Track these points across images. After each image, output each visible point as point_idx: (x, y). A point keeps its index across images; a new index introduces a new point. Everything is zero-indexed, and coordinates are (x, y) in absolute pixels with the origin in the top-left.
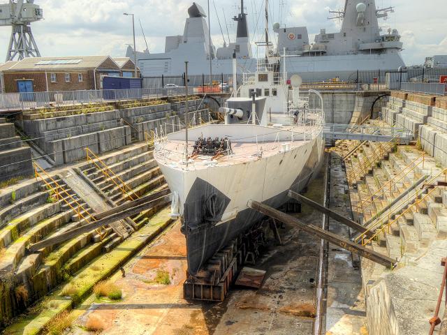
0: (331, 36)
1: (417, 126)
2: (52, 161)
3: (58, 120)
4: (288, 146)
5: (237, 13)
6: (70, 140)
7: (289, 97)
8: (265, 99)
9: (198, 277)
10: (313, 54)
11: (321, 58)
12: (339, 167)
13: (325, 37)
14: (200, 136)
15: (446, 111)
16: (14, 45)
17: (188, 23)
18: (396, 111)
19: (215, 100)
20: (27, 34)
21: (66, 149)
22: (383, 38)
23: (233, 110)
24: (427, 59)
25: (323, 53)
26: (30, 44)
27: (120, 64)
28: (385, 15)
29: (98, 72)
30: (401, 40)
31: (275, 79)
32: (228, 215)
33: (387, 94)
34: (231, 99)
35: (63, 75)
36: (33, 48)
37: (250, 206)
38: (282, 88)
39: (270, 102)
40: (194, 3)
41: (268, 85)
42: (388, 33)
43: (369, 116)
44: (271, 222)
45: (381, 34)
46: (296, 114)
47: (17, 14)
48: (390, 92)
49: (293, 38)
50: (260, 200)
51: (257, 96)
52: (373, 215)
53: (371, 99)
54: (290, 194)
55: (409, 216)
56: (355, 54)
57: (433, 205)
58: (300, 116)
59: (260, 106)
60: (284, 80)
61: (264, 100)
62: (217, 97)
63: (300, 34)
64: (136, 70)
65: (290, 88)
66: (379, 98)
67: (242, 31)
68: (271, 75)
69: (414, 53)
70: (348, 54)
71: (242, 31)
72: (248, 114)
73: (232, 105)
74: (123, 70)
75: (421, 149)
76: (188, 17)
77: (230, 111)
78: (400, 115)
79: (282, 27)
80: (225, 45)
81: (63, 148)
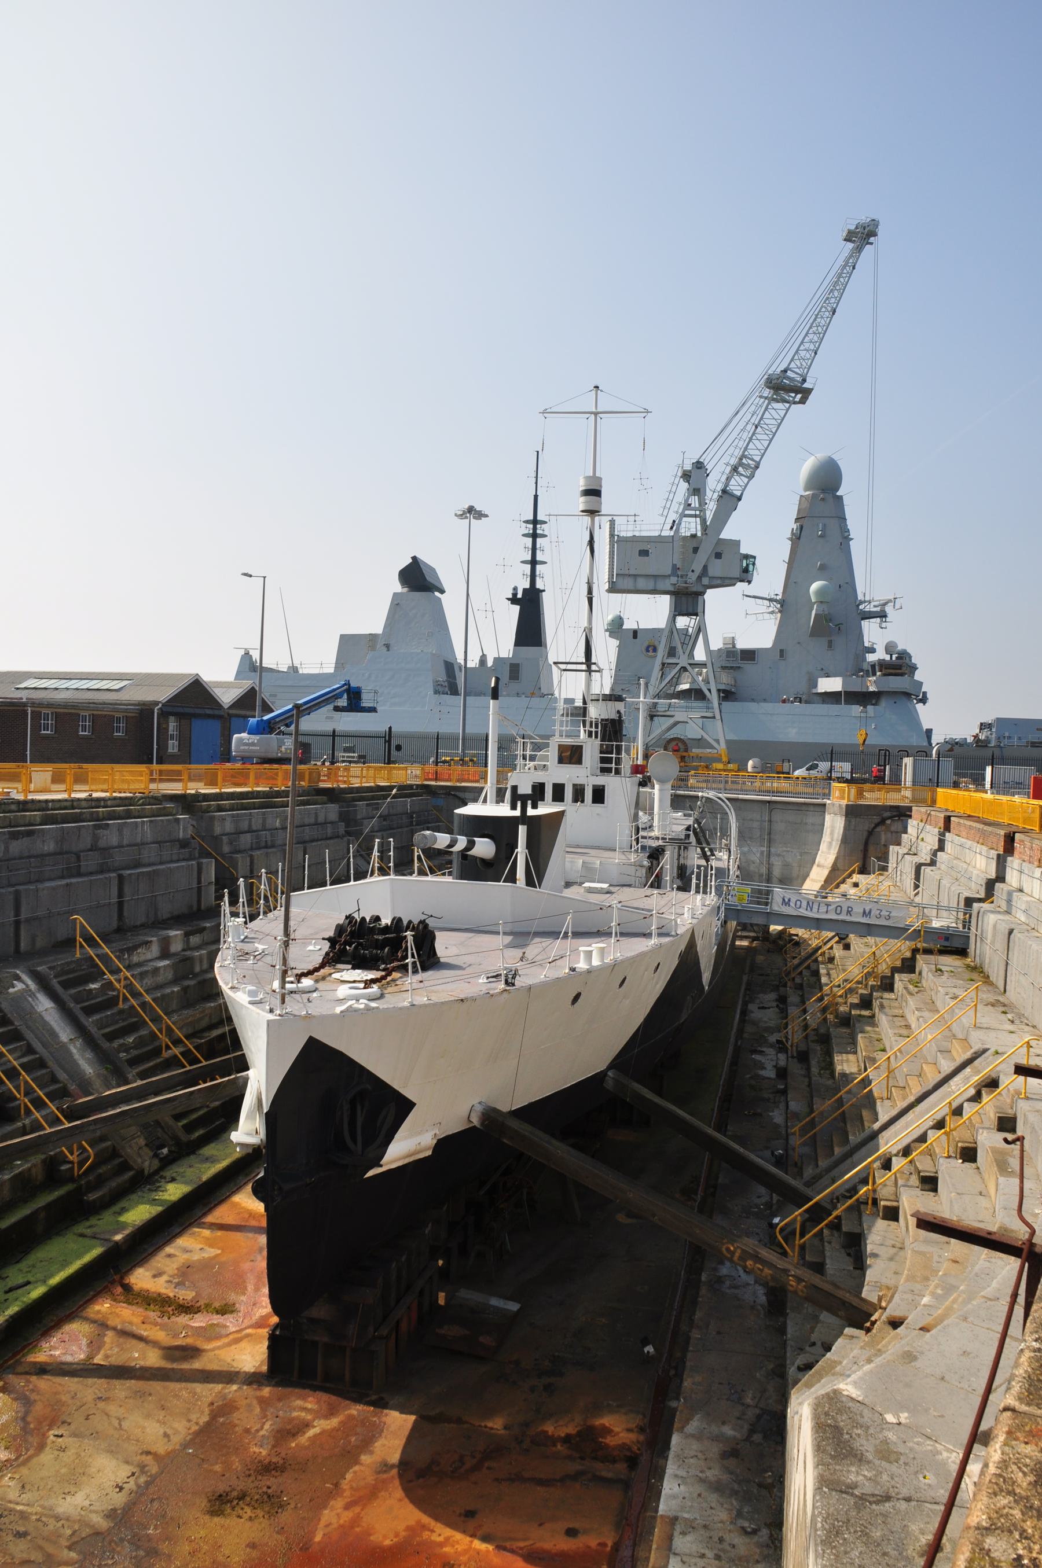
0: (749, 655)
1: (969, 902)
3: (14, 836)
4: (592, 955)
9: (312, 1321)
12: (770, 998)
15: (1037, 872)
17: (397, 603)
18: (924, 857)
21: (23, 916)
22: (873, 666)
24: (983, 726)
27: (227, 698)
28: (882, 615)
30: (918, 676)
31: (603, 760)
32: (406, 1146)
33: (902, 814)
37: (476, 1121)
38: (620, 788)
39: (578, 820)
40: (414, 558)
41: (585, 774)
42: (888, 658)
45: (871, 658)
48: (910, 809)
50: (505, 1108)
52: (823, 1163)
54: (609, 1084)
55: (926, 1166)
59: (543, 834)
61: (557, 818)
67: (530, 630)
69: (949, 715)
71: (530, 630)
72: (505, 848)
74: (231, 712)
75: (978, 970)
76: (398, 588)
81: (17, 913)
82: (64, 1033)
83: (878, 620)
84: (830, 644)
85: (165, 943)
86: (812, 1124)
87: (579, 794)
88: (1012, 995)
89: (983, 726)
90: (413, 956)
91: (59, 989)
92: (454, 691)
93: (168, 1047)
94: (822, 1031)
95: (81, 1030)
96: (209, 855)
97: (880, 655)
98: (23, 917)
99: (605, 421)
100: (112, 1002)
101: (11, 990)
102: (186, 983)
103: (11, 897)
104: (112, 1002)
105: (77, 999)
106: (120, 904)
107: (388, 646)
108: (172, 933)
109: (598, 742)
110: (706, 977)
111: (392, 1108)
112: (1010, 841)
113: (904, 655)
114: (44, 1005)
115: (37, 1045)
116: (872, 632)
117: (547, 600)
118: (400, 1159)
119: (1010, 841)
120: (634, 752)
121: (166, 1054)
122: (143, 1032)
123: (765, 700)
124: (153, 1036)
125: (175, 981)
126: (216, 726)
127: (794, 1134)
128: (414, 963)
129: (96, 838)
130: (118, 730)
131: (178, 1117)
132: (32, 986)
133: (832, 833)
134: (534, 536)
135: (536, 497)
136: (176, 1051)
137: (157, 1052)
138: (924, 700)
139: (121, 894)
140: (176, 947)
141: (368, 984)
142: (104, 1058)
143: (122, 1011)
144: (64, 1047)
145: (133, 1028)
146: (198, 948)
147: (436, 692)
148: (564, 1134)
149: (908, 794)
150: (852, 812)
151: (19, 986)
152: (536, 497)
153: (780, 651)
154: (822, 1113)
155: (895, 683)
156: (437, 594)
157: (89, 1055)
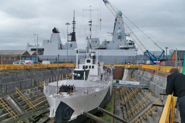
0: (108, 42)
2: (2, 92)
6: (25, 81)
7: (99, 69)
8: (89, 70)
11: (104, 50)
14: (63, 84)
17: (52, 35)
19: (69, 69)
23: (76, 74)
25: (105, 49)
31: (93, 62)
32: (74, 117)
34: (75, 70)
37: (82, 114)
40: (55, 28)
41: (91, 64)
43: (130, 77)
44: (91, 119)
46: (102, 76)
49: (92, 43)
51: (86, 69)
53: (131, 71)
54: (98, 109)
56: (117, 49)
57: (154, 113)
58: (103, 77)
59: (87, 72)
60: (97, 62)
62: (69, 68)
63: (96, 41)
64: (37, 56)
65: (99, 65)
66: (134, 70)
67: (73, 39)
68: (92, 60)
70: (115, 49)
73: (75, 72)
75: (150, 91)
76: (52, 32)
77: (75, 74)
78: (142, 77)
81: (7, 87)
82: (16, 105)
84: (121, 40)
85: (28, 91)
86: (127, 114)
88: (155, 94)
91: (14, 98)
92: (62, 49)
93: (30, 107)
94: (128, 101)
95: (18, 104)
96: (32, 78)
98: (7, 88)
99: (92, 11)
100: (22, 100)
102: (32, 97)
103: (6, 85)
104: (22, 100)
105: (17, 100)
106: (21, 86)
107: (51, 42)
108: (29, 90)
109: (92, 59)
111: (71, 111)
114: (12, 101)
115: (12, 107)
117: (76, 34)
120: (97, 60)
121: (30, 108)
122: (26, 105)
123: (111, 49)
124: (28, 105)
125: (30, 97)
127: (125, 116)
130: (4, 59)
131: (33, 117)
134: (74, 24)
135: (74, 18)
136: (32, 107)
137: (29, 108)
139: (21, 84)
140: (30, 92)
142: (21, 108)
143: (23, 102)
144: (16, 107)
145: (25, 104)
146: (33, 92)
147: (59, 49)
148: (95, 115)
151: (8, 98)
152: (74, 18)
154: (129, 113)
157: (19, 108)
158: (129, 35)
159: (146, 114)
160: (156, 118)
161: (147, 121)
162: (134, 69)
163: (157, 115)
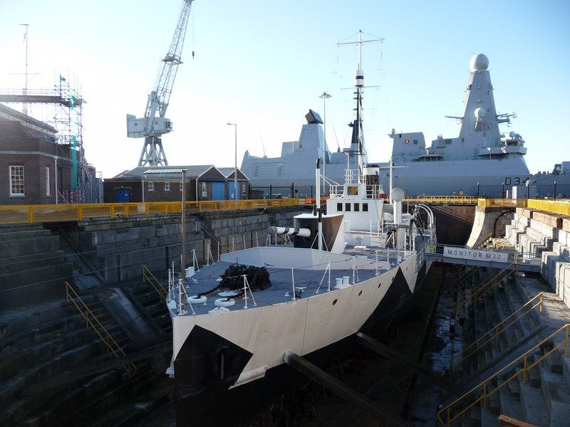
0: (449, 141)
2: (102, 278)
5: (353, 119)
10: (428, 158)
11: (437, 163)
13: (442, 143)
16: (145, 155)
20: (157, 146)
25: (440, 158)
26: (159, 155)
28: (508, 121)
29: (201, 180)
30: (525, 146)
31: (368, 193)
32: (248, 374)
35: (163, 184)
36: (162, 158)
41: (361, 198)
42: (511, 138)
47: (149, 128)
53: (494, 215)
57: (547, 377)
66: (503, 213)
68: (362, 188)
69: (539, 161)
70: (467, 159)
72: (314, 232)
79: (398, 132)
80: (339, 150)
81: (119, 264)
83: (506, 123)
87: (348, 208)
89: (556, 166)
90: (247, 286)
97: (508, 137)
98: (121, 265)
101: (111, 297)
110: (231, 387)
112: (560, 223)
113: (518, 136)
116: (503, 129)
118: (250, 379)
119: (560, 223)
126: (222, 186)
128: (247, 290)
129: (157, 232)
130: (151, 188)
132: (121, 295)
133: (479, 220)
138: (130, 119)
141: (229, 298)
149: (515, 202)
150: (488, 211)
153: (462, 139)
155: (512, 149)
156: (320, 124)
158: (508, 121)
159: (519, 371)
160: (553, 403)
161: (519, 401)
162: (503, 211)
163: (559, 391)
